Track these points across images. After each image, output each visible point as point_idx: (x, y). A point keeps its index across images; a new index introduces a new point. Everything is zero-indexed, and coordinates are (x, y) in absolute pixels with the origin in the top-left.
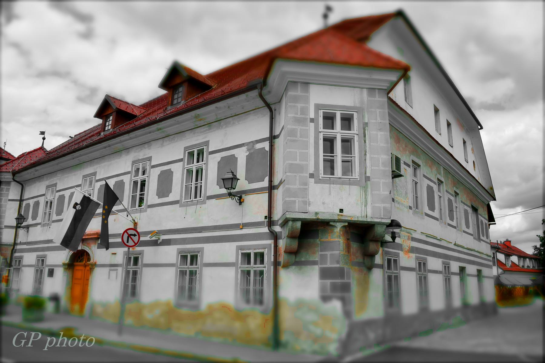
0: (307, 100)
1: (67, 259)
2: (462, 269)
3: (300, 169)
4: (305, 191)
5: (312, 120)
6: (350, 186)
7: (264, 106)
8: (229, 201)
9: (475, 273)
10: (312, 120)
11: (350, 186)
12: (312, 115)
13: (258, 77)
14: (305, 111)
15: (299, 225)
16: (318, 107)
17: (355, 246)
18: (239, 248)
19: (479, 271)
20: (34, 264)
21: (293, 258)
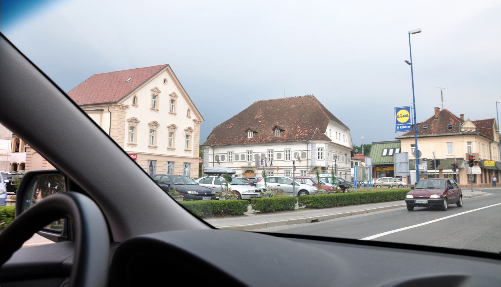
0: (315, 146)
1: (452, 156)
2: (341, 173)
3: (314, 158)
4: (315, 162)
5: (324, 150)
6: (434, 157)
7: (35, 153)
8: (217, 164)
9: (345, 174)
10: (324, 150)
11: (434, 157)
12: (316, 149)
13: (269, 137)
14: (315, 148)
15: (314, 167)
16: (317, 147)
17: (322, 170)
18: (300, 170)
19: (346, 173)
20: (472, 152)
21: (312, 173)
